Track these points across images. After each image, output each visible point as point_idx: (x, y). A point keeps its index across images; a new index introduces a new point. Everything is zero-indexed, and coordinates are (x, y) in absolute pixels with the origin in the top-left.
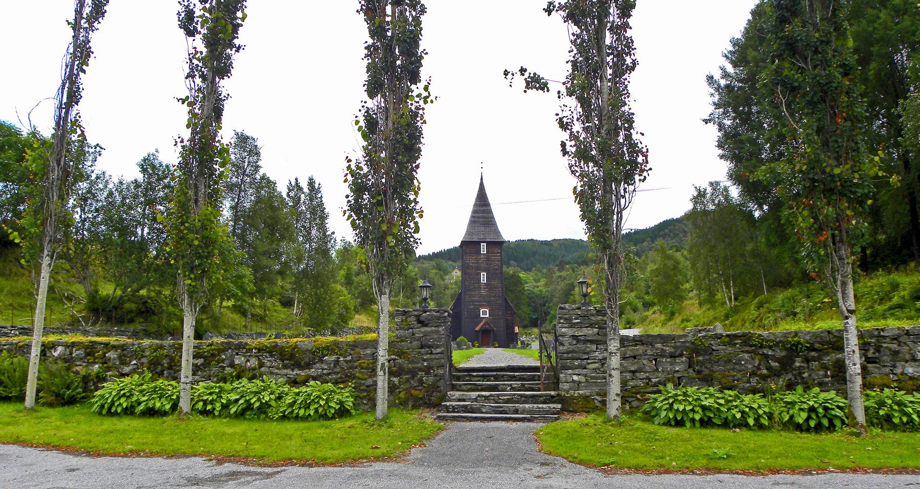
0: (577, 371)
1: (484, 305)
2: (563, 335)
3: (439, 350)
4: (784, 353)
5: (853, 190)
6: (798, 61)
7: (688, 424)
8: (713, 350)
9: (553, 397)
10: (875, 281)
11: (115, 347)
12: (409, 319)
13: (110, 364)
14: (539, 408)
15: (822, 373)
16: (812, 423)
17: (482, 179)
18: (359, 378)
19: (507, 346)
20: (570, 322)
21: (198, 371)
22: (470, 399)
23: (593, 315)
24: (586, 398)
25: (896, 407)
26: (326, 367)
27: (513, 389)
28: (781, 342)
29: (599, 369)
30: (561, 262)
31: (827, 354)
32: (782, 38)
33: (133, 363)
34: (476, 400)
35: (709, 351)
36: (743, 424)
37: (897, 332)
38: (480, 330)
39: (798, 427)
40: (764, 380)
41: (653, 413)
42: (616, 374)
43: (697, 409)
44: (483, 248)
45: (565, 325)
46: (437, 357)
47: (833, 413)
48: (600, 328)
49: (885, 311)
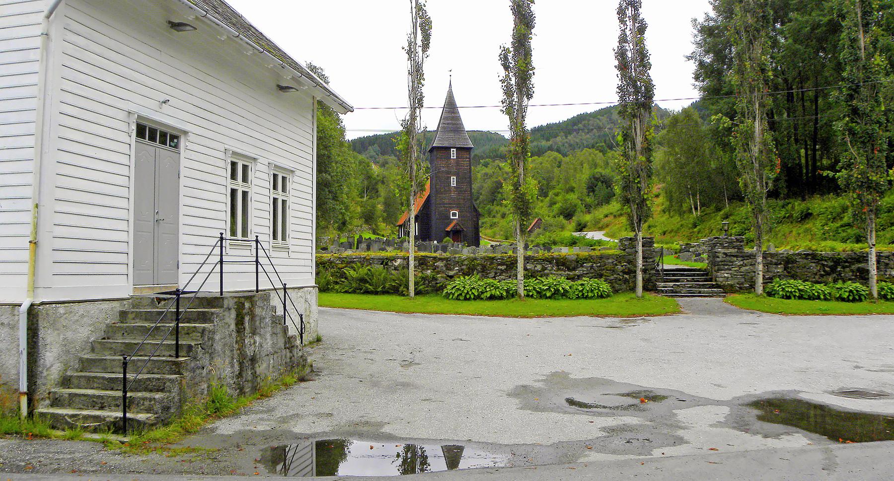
1: (453, 207)
3: (651, 260)
4: (832, 264)
5: (880, 187)
6: (856, 117)
7: (793, 298)
8: (797, 261)
9: (714, 285)
10: (829, 204)
11: (441, 259)
13: (439, 270)
15: (851, 274)
16: (851, 298)
18: (606, 276)
21: (502, 273)
22: (670, 287)
23: (734, 242)
24: (731, 286)
25: (889, 291)
26: (585, 270)
27: (688, 281)
28: (831, 258)
29: (738, 271)
31: (854, 264)
32: (850, 106)
33: (456, 269)
34: (672, 287)
35: (795, 262)
36: (818, 298)
37: (888, 254)
38: (451, 231)
39: (843, 300)
40: (822, 277)
41: (773, 293)
42: (761, 273)
43: (797, 291)
44: (453, 153)
46: (650, 263)
47: (861, 293)
48: (738, 249)
49: (837, 228)
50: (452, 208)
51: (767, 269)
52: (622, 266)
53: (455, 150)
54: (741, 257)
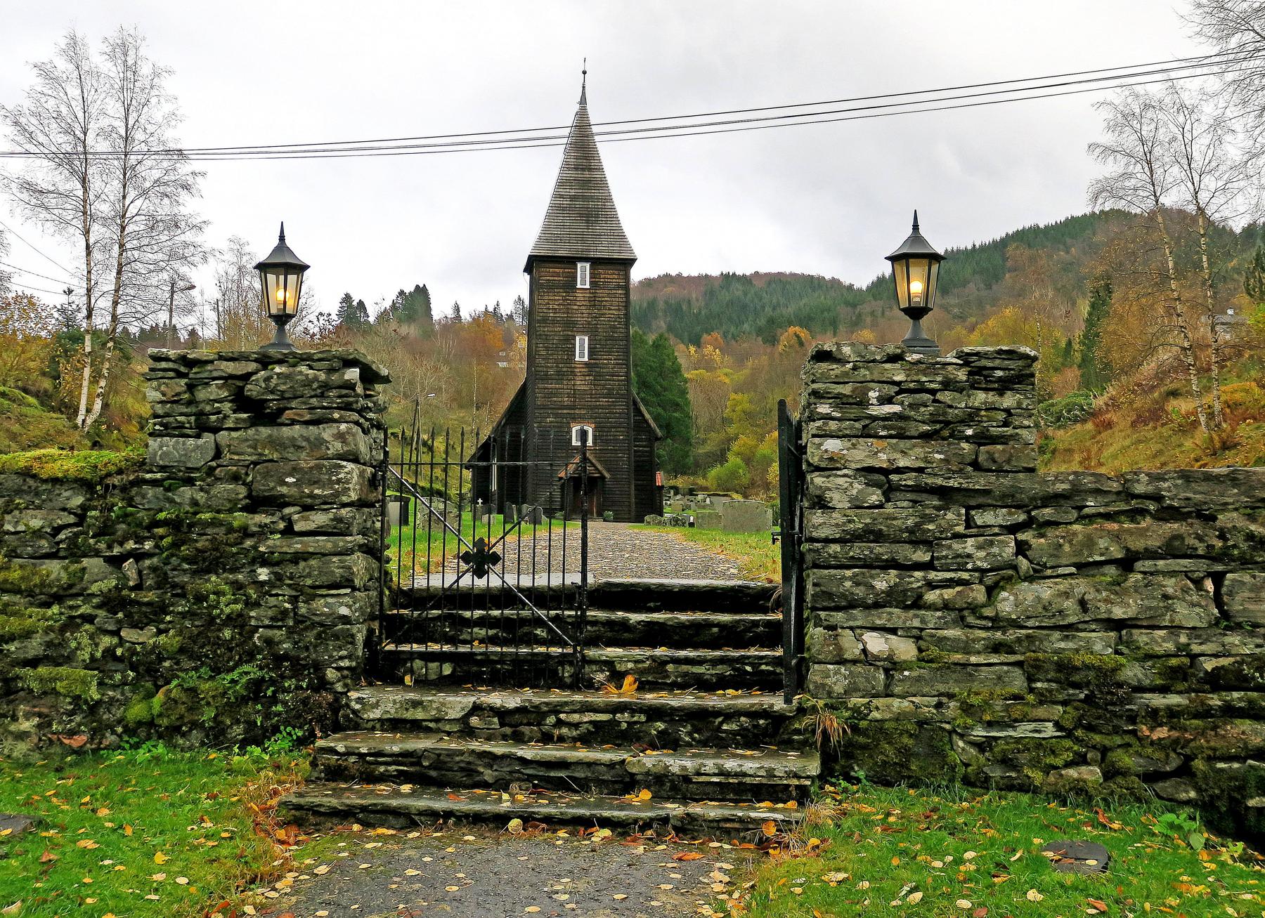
0: (881, 619)
2: (831, 466)
3: (320, 519)
9: (778, 720)
12: (201, 394)
14: (727, 774)
17: (583, 101)
19: (639, 519)
20: (854, 411)
30: (771, 321)
44: (583, 273)
45: (833, 425)
46: (313, 544)
47: (977, 364)
50: (575, 418)
51: (1218, 599)
52: (116, 562)
53: (588, 265)
54: (1009, 500)
